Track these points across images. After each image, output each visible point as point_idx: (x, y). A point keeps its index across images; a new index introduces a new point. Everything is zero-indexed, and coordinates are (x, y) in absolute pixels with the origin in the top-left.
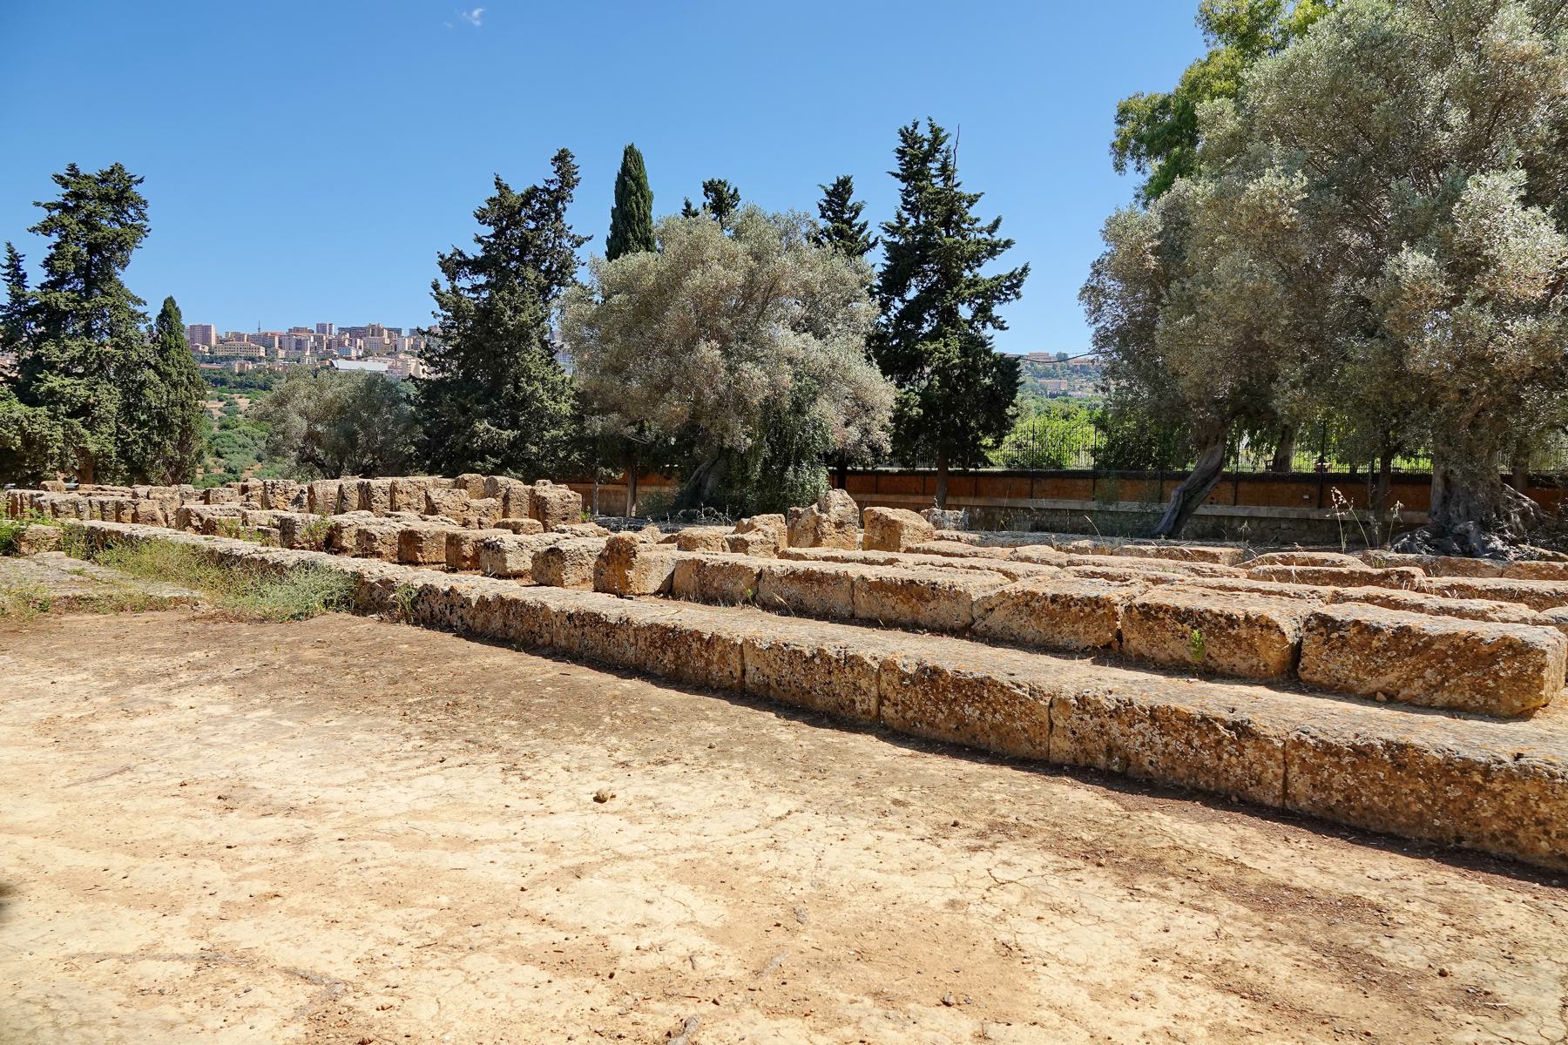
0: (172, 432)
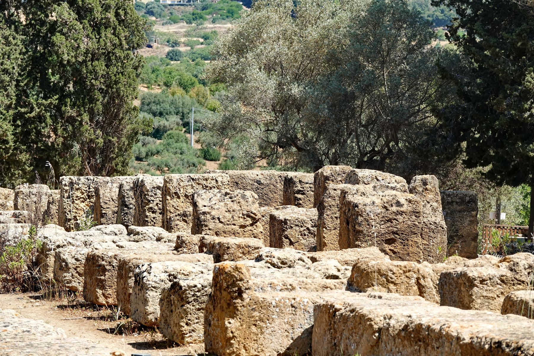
0: (92, 100)
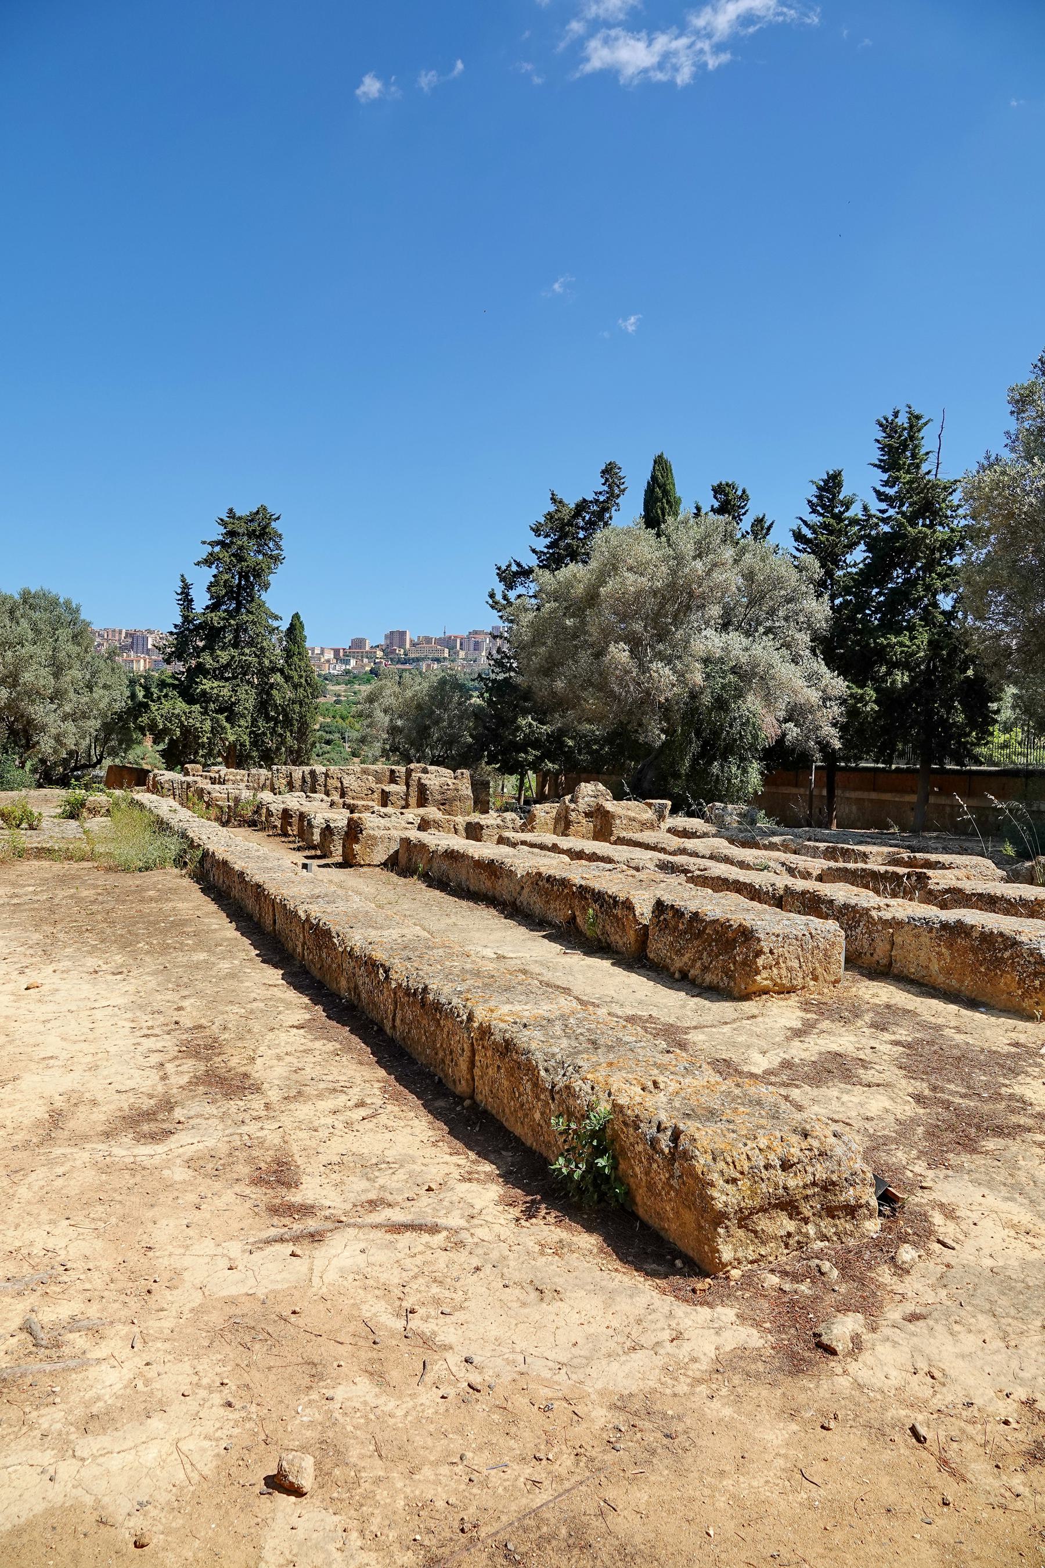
0: (292, 725)
